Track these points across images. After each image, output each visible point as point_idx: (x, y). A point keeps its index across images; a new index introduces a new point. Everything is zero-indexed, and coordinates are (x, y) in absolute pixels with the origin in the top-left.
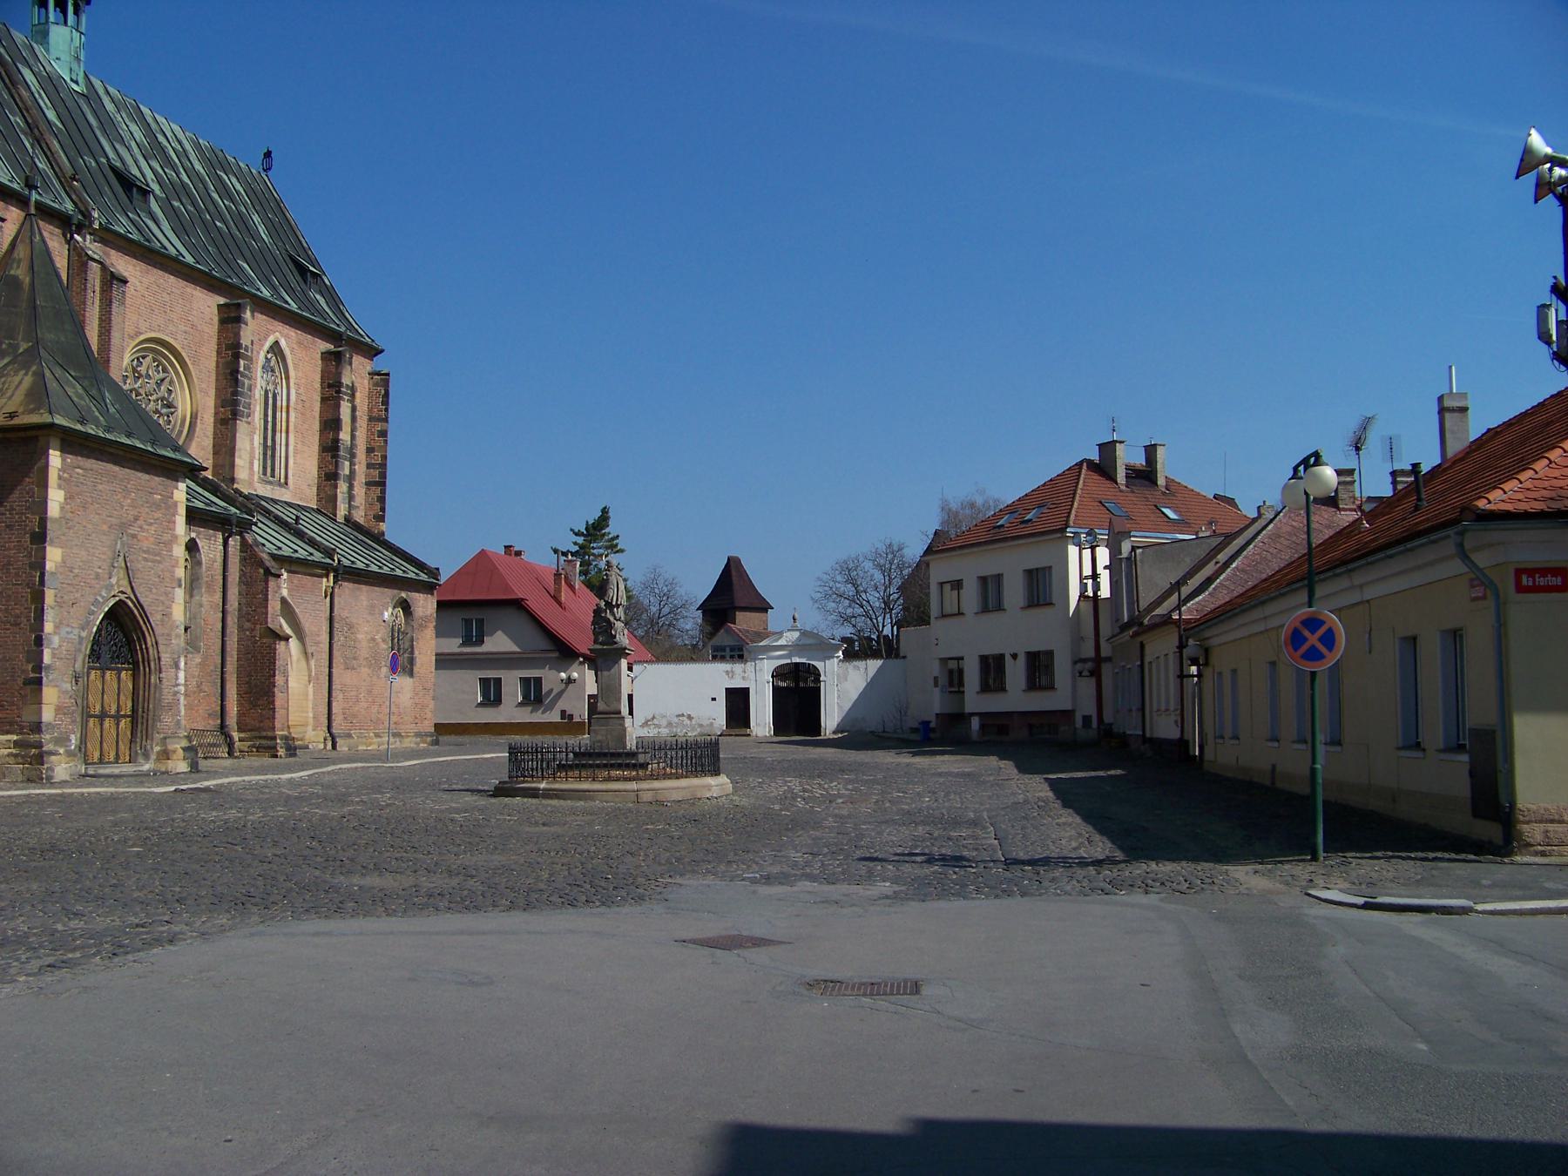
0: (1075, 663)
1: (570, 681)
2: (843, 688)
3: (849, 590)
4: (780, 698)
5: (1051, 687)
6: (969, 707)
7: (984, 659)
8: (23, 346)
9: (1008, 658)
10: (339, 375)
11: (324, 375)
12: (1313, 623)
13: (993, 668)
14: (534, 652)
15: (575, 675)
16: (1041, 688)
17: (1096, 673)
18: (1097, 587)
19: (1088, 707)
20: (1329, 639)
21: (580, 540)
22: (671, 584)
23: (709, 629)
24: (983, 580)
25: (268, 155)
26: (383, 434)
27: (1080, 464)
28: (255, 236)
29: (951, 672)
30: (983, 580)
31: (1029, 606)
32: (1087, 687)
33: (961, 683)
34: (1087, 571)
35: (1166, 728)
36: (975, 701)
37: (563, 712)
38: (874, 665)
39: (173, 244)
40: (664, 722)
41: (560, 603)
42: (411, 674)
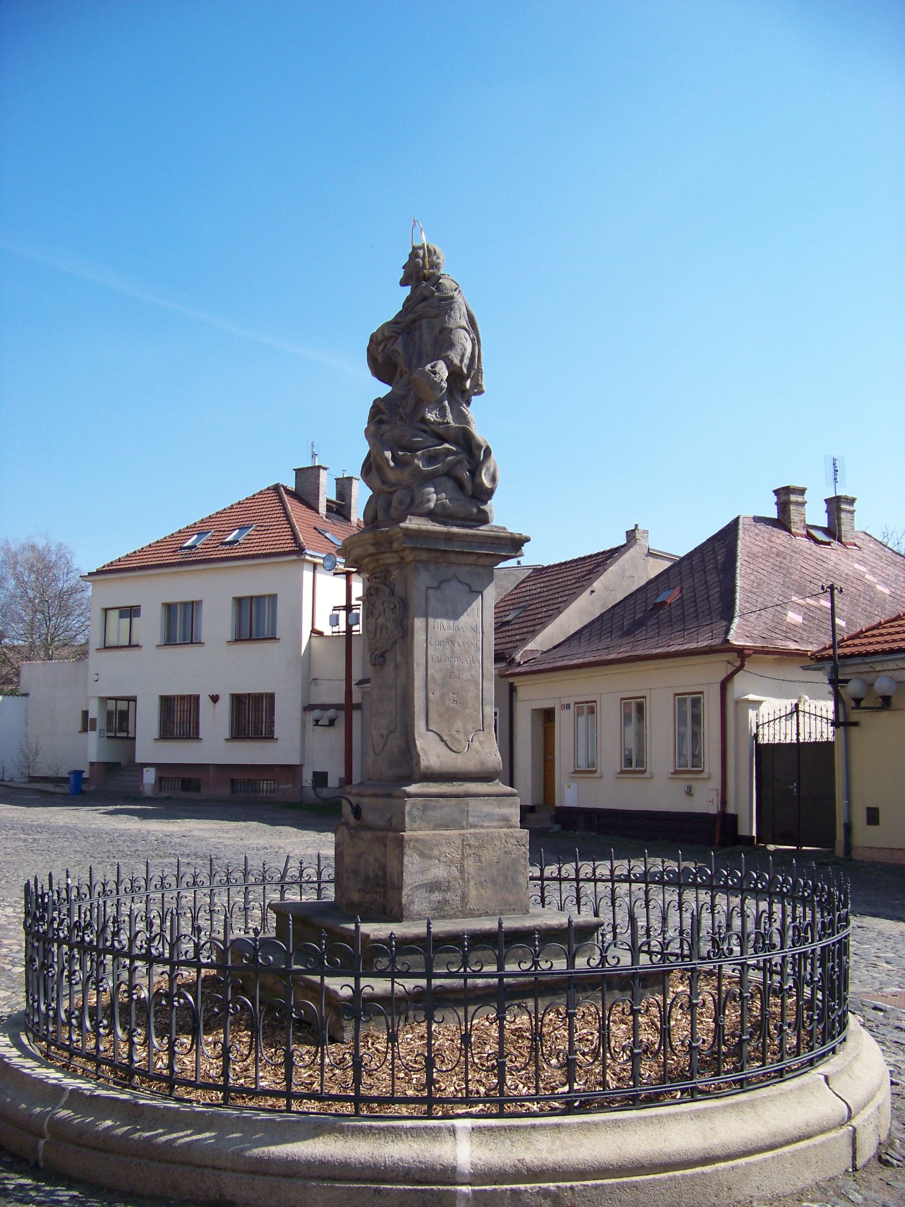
7: (167, 703)
13: (179, 716)
24: (169, 608)
30: (169, 608)
31: (236, 640)
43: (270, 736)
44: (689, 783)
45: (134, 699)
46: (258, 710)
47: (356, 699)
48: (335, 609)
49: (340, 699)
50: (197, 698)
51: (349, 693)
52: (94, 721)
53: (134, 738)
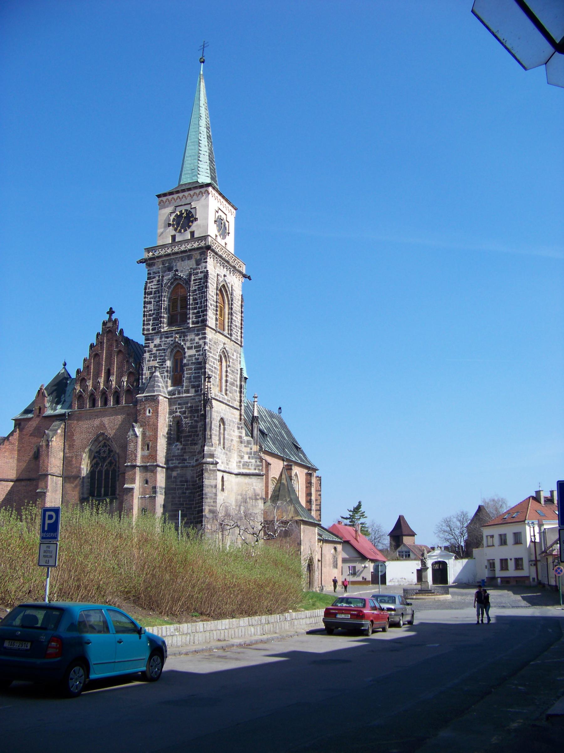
0: (529, 561)
1: (365, 567)
2: (455, 568)
3: (448, 529)
4: (435, 572)
5: (522, 569)
6: (497, 575)
8: (288, 500)
9: (509, 560)
10: (311, 480)
11: (306, 480)
12: (559, 568)
13: (504, 563)
14: (353, 557)
15: (367, 565)
16: (519, 569)
17: (536, 565)
18: (535, 539)
19: (534, 575)
20: (561, 571)
21: (351, 513)
22: (379, 526)
23: (394, 543)
25: (280, 408)
26: (320, 495)
27: (530, 498)
28: (285, 439)
29: (490, 563)
30: (500, 535)
32: (533, 569)
33: (494, 567)
34: (532, 534)
35: (553, 582)
36: (499, 573)
37: (363, 578)
38: (465, 561)
39: (276, 451)
40: (396, 580)
41: (357, 540)
42: (337, 568)
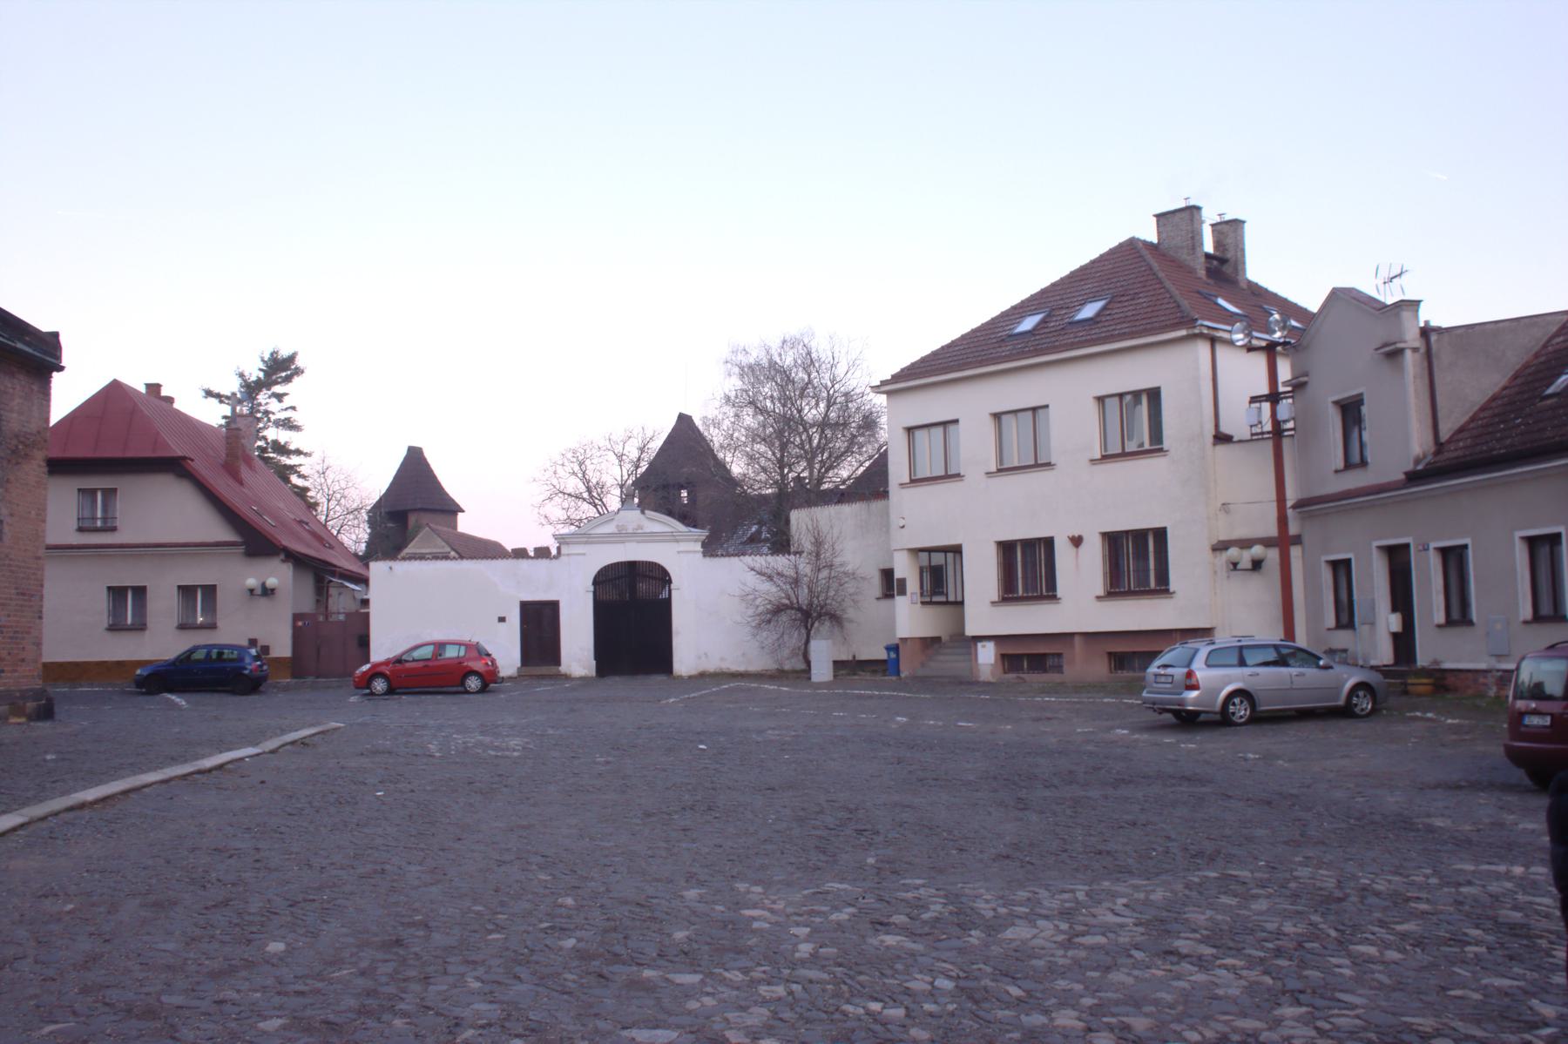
13: (1028, 567)
43: (1163, 588)
44: (1342, 639)
45: (957, 550)
46: (1141, 554)
47: (1293, 529)
48: (1254, 400)
49: (1272, 530)
50: (1049, 543)
51: (1282, 521)
52: (902, 582)
53: (962, 603)
